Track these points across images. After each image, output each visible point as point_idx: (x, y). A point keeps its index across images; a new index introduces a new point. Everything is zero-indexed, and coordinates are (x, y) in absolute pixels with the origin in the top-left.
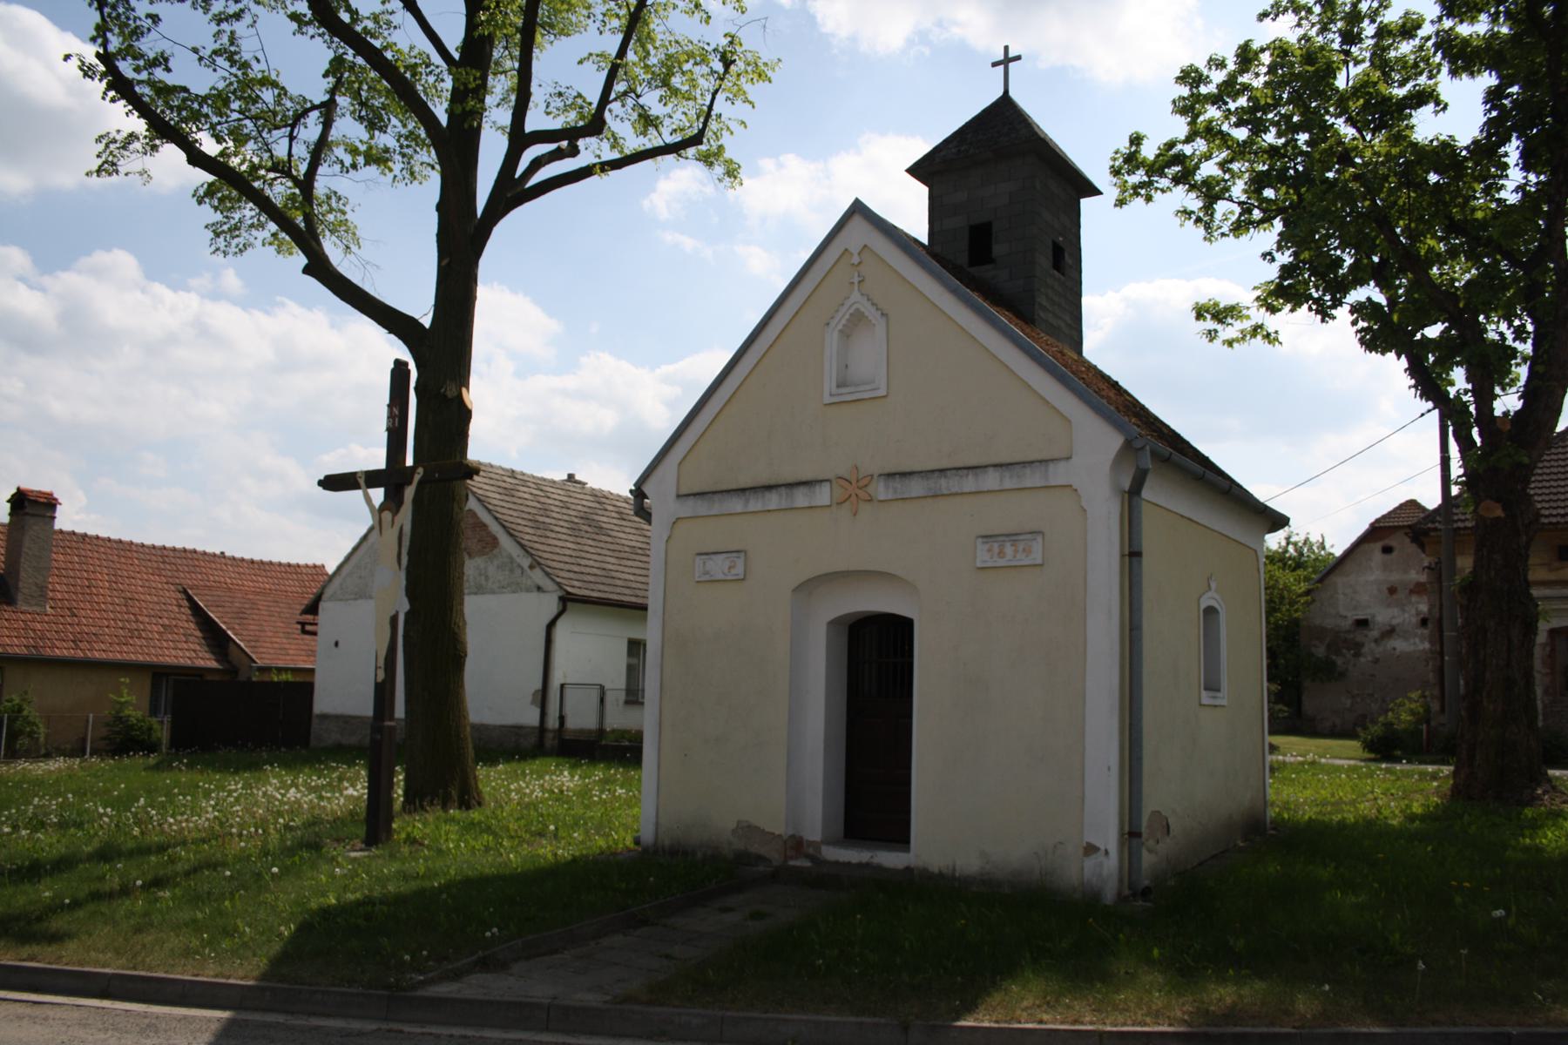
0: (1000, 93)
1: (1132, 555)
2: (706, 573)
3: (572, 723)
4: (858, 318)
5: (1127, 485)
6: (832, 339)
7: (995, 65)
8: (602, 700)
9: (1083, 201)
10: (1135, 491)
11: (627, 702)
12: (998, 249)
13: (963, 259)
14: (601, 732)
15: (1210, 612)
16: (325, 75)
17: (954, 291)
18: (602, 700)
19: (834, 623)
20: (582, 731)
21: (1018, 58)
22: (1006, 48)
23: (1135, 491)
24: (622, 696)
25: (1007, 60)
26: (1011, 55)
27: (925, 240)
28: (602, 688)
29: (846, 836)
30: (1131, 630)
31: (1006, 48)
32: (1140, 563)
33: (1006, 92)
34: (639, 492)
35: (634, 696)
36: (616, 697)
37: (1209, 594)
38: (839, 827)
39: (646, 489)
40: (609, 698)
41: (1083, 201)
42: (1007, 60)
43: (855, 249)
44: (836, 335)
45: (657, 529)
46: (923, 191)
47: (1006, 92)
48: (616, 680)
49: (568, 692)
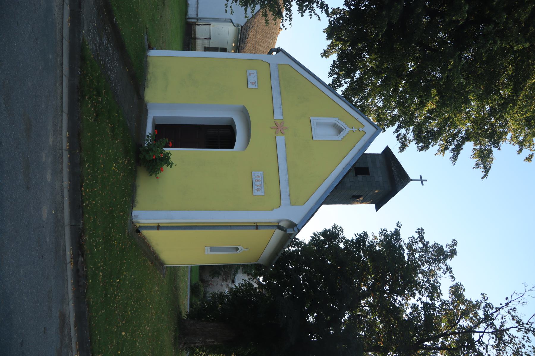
0: (411, 178)
1: (256, 227)
2: (250, 74)
3: (198, 28)
4: (340, 130)
5: (281, 224)
6: (333, 120)
7: (421, 176)
8: (205, 39)
9: (374, 205)
10: (279, 227)
11: (205, 47)
12: (360, 177)
13: (357, 166)
14: (195, 39)
15: (237, 249)
16: (326, 54)
17: (349, 163)
18: (205, 39)
19: (232, 120)
20: (195, 32)
21: (423, 184)
22: (426, 180)
23: (279, 227)
24: (207, 46)
25: (422, 180)
26: (424, 182)
27: (366, 152)
28: (210, 39)
29: (156, 124)
30: (230, 226)
31: (426, 180)
32: (254, 229)
33: (412, 180)
34: (279, 50)
35: (208, 49)
36: (207, 43)
37: (243, 248)
38: (157, 122)
39: (280, 52)
40: (206, 41)
41: (374, 205)
42: (422, 180)
43: (364, 129)
44: (335, 122)
45: (266, 57)
46: (380, 152)
47: (412, 180)
48: (212, 44)
49: (208, 27)
